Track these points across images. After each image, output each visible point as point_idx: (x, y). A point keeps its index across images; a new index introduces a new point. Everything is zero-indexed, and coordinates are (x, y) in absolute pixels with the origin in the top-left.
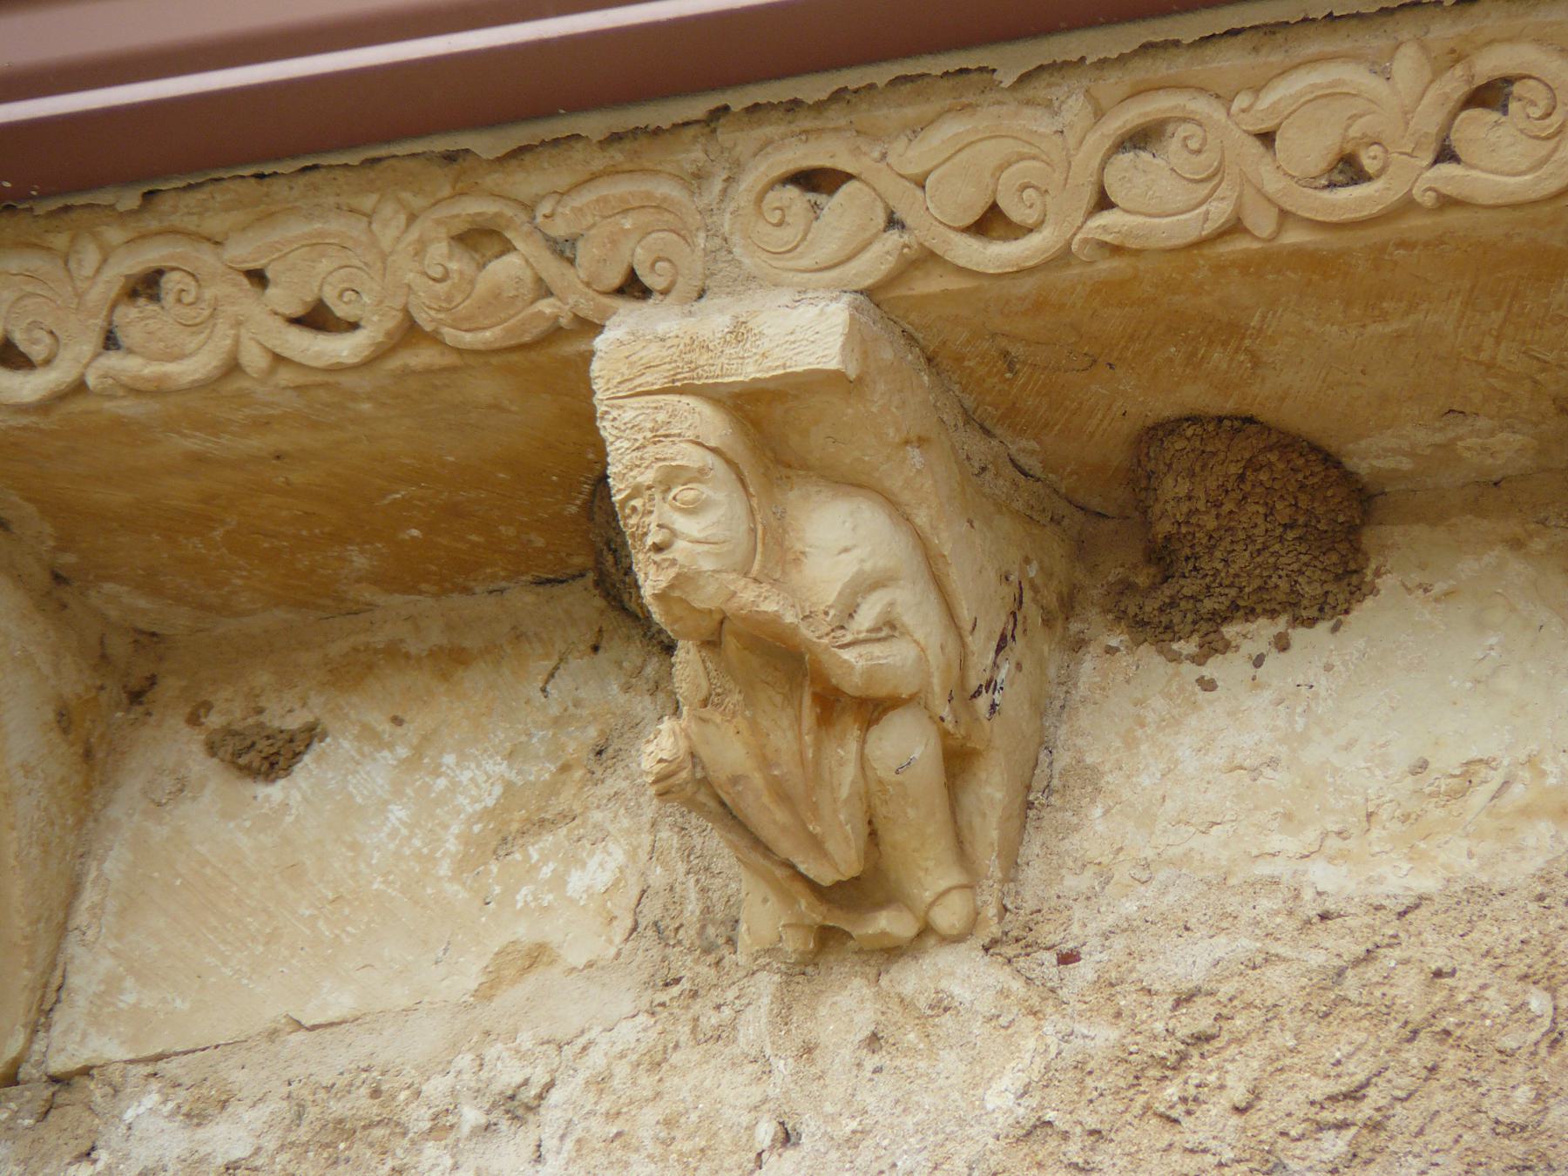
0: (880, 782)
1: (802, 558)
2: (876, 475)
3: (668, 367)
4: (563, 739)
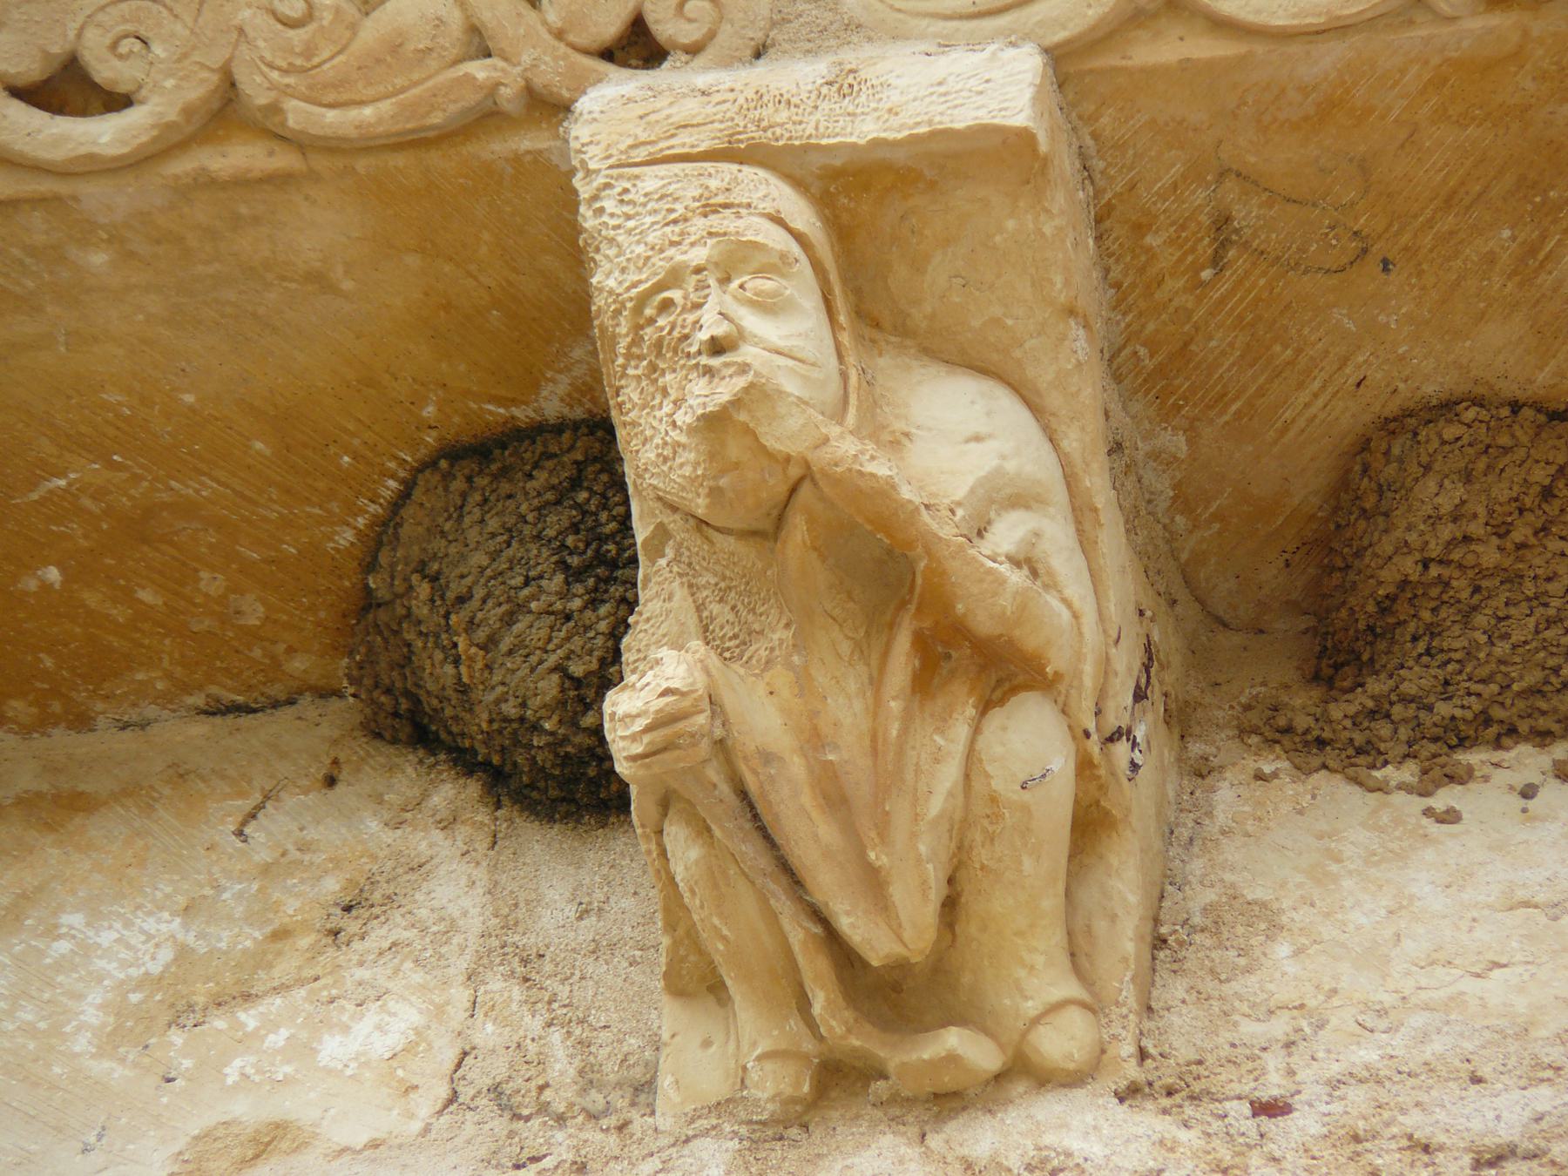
0: (994, 799)
1: (905, 441)
2: (1018, 353)
3: (717, 125)
4: (276, 895)
